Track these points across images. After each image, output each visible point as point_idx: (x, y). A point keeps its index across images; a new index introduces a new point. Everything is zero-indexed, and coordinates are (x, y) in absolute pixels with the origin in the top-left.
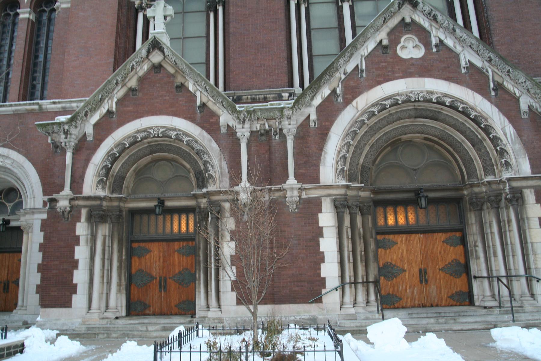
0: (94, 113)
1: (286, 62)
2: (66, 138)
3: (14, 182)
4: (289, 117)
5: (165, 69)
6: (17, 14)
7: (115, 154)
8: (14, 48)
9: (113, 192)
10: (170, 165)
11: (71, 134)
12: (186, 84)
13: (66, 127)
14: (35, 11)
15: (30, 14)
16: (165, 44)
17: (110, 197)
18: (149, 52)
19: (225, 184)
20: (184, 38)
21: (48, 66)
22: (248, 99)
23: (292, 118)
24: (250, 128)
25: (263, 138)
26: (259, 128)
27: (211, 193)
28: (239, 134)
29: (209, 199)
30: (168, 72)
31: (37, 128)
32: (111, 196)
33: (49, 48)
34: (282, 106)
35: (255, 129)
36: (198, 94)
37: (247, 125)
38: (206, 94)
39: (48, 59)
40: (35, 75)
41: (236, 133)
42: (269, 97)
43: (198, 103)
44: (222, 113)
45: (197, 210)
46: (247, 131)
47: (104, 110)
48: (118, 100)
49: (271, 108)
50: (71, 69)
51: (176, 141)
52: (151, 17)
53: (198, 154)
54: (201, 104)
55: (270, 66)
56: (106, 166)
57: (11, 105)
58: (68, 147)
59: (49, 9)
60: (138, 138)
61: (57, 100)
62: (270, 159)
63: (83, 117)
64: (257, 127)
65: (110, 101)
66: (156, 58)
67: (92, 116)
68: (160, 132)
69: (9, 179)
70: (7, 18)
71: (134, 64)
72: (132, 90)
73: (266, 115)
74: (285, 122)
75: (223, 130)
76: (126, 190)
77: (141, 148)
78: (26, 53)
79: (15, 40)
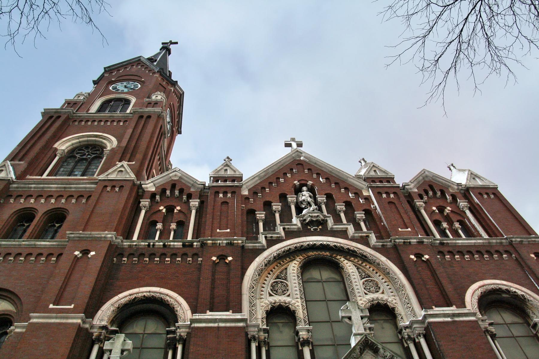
21: (523, 256)
52: (107, 350)
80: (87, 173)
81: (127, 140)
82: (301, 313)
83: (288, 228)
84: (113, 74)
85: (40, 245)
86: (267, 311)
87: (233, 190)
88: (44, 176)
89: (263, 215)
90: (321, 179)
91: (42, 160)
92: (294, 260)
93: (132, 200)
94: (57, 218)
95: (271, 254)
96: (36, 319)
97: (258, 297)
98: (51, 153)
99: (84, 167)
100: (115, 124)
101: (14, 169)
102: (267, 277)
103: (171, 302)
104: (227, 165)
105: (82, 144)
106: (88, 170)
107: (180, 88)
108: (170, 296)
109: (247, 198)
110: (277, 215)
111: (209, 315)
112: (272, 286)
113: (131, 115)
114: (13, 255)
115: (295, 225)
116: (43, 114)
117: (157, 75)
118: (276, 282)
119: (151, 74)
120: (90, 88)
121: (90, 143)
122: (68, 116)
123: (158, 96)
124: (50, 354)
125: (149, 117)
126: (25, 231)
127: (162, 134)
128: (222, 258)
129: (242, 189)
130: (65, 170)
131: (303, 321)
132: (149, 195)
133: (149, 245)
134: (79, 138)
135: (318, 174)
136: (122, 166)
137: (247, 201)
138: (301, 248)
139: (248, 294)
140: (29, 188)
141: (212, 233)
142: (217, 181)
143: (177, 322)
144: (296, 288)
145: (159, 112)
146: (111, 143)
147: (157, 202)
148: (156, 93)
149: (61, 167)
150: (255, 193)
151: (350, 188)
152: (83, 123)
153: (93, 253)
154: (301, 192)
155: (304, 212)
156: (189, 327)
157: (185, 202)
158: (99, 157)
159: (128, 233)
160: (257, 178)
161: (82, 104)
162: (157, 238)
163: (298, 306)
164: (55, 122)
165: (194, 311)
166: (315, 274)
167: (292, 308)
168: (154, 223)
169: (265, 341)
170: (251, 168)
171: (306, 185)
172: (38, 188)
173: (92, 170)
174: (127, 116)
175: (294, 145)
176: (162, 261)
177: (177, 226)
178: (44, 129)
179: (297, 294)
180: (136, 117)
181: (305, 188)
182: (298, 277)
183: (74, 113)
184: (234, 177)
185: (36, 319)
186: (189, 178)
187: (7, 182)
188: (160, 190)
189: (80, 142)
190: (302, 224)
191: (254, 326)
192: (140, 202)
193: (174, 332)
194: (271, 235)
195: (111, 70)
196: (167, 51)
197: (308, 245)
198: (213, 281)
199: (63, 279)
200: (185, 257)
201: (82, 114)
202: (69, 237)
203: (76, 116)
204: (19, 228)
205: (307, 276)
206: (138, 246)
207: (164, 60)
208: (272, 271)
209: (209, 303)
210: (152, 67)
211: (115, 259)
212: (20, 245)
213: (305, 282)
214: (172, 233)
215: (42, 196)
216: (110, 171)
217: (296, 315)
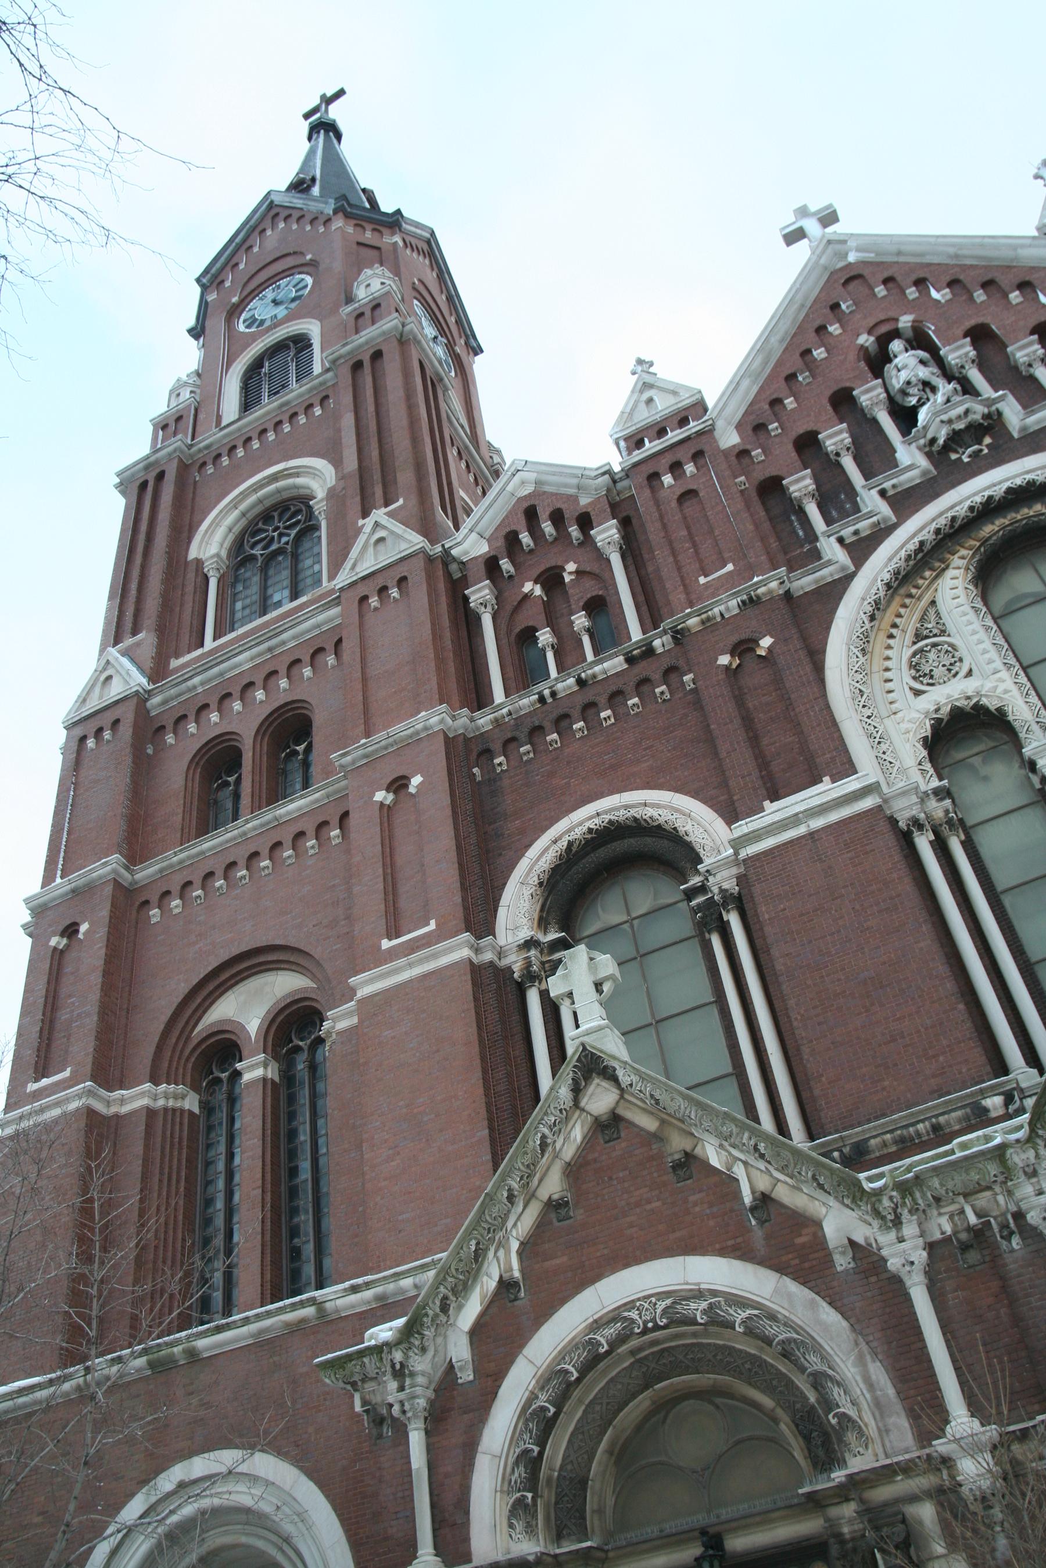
0: (466, 1298)
1: (961, 1006)
2: (401, 1388)
3: (273, 1552)
4: (1029, 1170)
5: (630, 1124)
6: (238, 1074)
7: (543, 1409)
8: (237, 1160)
9: (559, 1537)
10: (711, 1408)
11: (412, 1375)
12: (698, 1151)
13: (398, 1356)
14: (276, 1057)
15: (266, 1066)
16: (614, 1058)
17: (556, 1556)
18: (577, 1091)
19: (900, 1439)
20: (657, 1022)
22: (885, 1144)
23: (1041, 1171)
24: (922, 1235)
25: (973, 1256)
26: (948, 1229)
27: (864, 1481)
28: (894, 1264)
29: (862, 1501)
30: (642, 1129)
31: (322, 1374)
32: (558, 1551)
33: (321, 1141)
34: (998, 1141)
35: (938, 1236)
36: (739, 1171)
37: (910, 1229)
38: (762, 1165)
39: (323, 1171)
40: (296, 1220)
41: (885, 1261)
42: (948, 1124)
43: (748, 1199)
44: (824, 1210)
45: (834, 1550)
46: (915, 1248)
47: (489, 1283)
48: (522, 1243)
49: (966, 1158)
50: (384, 1184)
51: (712, 1329)
52: (561, 997)
53: (786, 1355)
54: (755, 1199)
55: (919, 1031)
56: (526, 1452)
57: (246, 1321)
58: (410, 1414)
59: (309, 1042)
60: (599, 1344)
61: (360, 1281)
62: (1017, 1320)
63: (436, 1316)
64: (942, 1225)
65: (501, 1253)
66: (600, 1099)
67: (460, 1307)
68: (659, 1311)
69: (260, 1544)
70: (214, 1091)
71: (546, 1131)
72: (554, 1206)
73: (958, 1181)
74: (1026, 1190)
75: (842, 1262)
76: (596, 1522)
77: (613, 1374)
78: (268, 1168)
79: (237, 1142)
80: (301, 586)
81: (354, 448)
82: (1021, 709)
83: (894, 486)
84: (228, 284)
85: (289, 813)
86: (925, 739)
87: (693, 451)
88: (209, 644)
89: (845, 435)
90: (934, 294)
91: (182, 605)
92: (947, 567)
93: (443, 600)
94: (290, 732)
95: (875, 580)
96: (368, 984)
97: (884, 714)
98: (191, 575)
99: (286, 573)
100: (302, 419)
101: (133, 660)
102: (889, 647)
103: (661, 820)
104: (647, 386)
105: (250, 515)
106: (301, 577)
107: (417, 225)
108: (654, 806)
109: (743, 454)
110: (848, 463)
111: (774, 811)
112: (912, 666)
113: (330, 375)
114: (242, 862)
115: (910, 467)
116: (123, 486)
117: (338, 223)
118: (921, 651)
119: (322, 229)
120: (190, 355)
121: (268, 503)
122: (181, 460)
123: (373, 283)
124: (438, 1051)
125: (377, 355)
126: (237, 796)
127: (433, 385)
128: (744, 648)
129: (717, 434)
130: (248, 601)
131: (1035, 727)
132: (482, 569)
133: (542, 699)
134: (235, 504)
135: (920, 283)
136: (377, 524)
137: (746, 461)
138: (952, 526)
139: (854, 714)
140: (190, 690)
141: (687, 594)
142: (640, 444)
143: (701, 861)
144: (981, 646)
145: (396, 328)
146: (318, 477)
147: (511, 577)
148: (362, 277)
149: (234, 602)
150: (760, 428)
151: (1033, 278)
152: (225, 461)
153: (416, 780)
154: (890, 361)
155: (922, 416)
156: (736, 861)
157: (581, 544)
158: (310, 528)
159: (477, 692)
160: (746, 383)
161: (196, 410)
162: (553, 672)
163: (1006, 692)
164: (161, 496)
165: (731, 817)
166: (1023, 581)
167: (992, 704)
168: (528, 635)
169: (950, 822)
170: (714, 356)
171: (896, 334)
172: (210, 680)
173: (309, 572)
174: (321, 384)
175: (812, 226)
176: (594, 725)
177: (589, 615)
178: (144, 527)
179: (990, 662)
180: (346, 371)
181: (896, 346)
182: (976, 610)
183: (192, 446)
184: (679, 411)
185: (368, 984)
186: (561, 474)
187: (135, 700)
188: (501, 543)
189: (244, 514)
190: (929, 455)
191: (904, 793)
192: (466, 599)
193: (702, 889)
194: (852, 529)
195: (215, 276)
196: (327, 132)
197: (971, 509)
198: (747, 721)
199: (381, 870)
200: (645, 688)
201: (210, 437)
202: (342, 766)
203: (200, 451)
204: (221, 795)
205: (1002, 596)
206: (517, 711)
207: (335, 164)
208: (894, 626)
209: (760, 782)
210: (314, 207)
211: (475, 770)
212: (245, 834)
213: (1002, 617)
214: (586, 640)
215: (228, 695)
216: (354, 553)
217: (1011, 718)
